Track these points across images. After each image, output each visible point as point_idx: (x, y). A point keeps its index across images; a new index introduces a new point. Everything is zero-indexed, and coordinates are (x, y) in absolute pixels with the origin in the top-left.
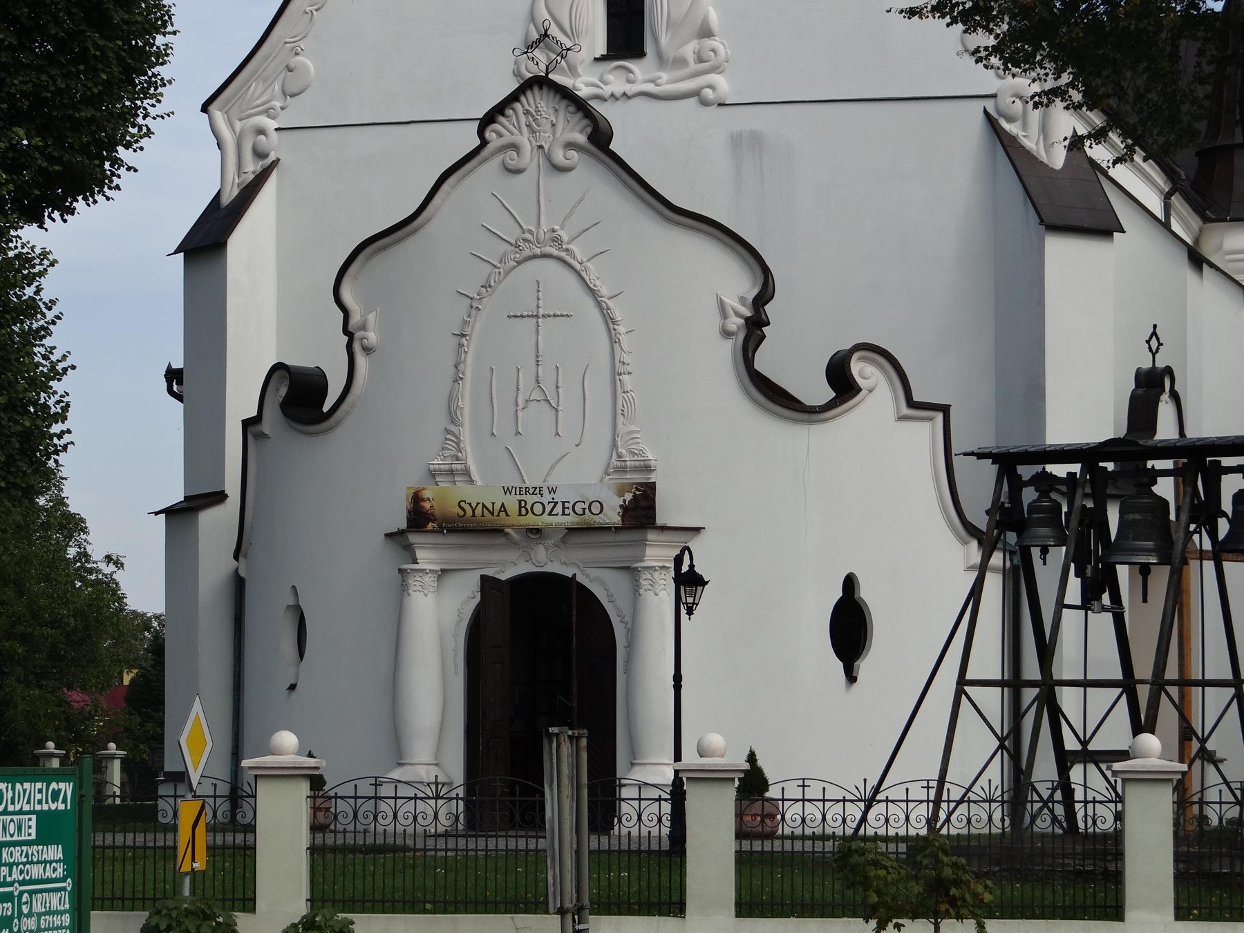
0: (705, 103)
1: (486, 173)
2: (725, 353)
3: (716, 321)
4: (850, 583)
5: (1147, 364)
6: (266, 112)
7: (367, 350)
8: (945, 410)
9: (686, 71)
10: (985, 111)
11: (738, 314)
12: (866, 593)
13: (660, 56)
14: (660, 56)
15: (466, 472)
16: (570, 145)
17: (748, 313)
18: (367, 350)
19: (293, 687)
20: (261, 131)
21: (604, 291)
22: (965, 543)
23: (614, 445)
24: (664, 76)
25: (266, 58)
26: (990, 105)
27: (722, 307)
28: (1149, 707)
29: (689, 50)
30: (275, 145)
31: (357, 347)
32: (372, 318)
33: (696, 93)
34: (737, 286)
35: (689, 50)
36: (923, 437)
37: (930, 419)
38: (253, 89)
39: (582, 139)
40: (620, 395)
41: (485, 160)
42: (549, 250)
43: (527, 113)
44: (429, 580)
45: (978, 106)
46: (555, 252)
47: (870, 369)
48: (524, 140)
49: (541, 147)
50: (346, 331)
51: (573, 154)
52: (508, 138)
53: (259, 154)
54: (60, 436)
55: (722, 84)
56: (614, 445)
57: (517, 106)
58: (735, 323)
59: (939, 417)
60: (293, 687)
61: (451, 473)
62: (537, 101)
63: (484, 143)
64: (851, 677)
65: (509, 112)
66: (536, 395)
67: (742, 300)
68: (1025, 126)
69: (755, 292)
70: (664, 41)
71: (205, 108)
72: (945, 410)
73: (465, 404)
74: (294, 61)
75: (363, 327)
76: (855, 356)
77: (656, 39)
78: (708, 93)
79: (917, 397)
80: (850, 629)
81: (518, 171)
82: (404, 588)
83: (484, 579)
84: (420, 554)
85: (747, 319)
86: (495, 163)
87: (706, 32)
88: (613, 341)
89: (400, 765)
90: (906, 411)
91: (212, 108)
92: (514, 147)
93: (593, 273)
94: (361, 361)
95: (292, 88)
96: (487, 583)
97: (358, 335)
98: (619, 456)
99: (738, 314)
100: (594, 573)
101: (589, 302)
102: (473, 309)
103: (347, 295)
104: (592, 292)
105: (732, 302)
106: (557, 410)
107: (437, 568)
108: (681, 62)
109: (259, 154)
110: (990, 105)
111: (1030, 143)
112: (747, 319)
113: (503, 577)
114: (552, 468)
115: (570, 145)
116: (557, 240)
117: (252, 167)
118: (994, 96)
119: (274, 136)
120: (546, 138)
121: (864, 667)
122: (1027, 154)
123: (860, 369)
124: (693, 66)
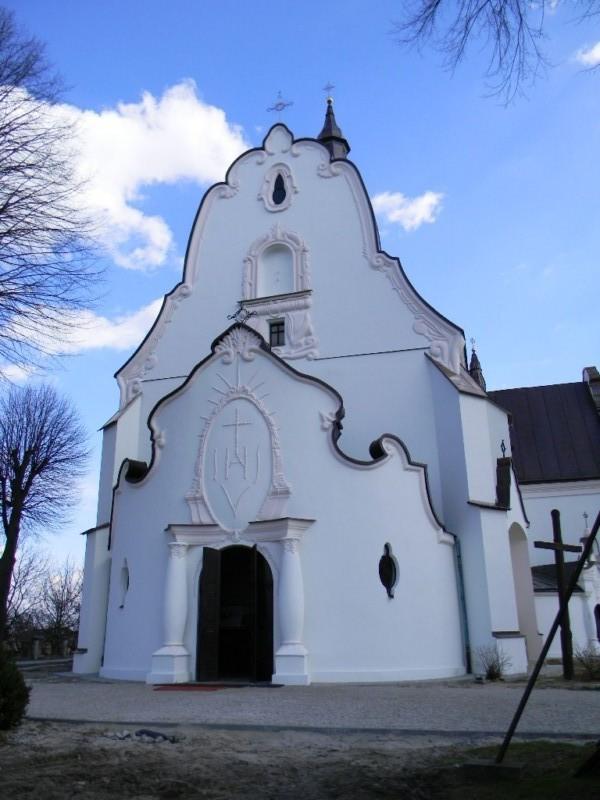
0: (309, 359)
1: (214, 366)
2: (323, 439)
3: (318, 424)
4: (387, 547)
5: (501, 456)
6: (138, 376)
7: (161, 447)
8: (425, 467)
9: (300, 349)
10: (426, 355)
11: (329, 420)
12: (395, 553)
13: (291, 344)
14: (291, 344)
15: (202, 498)
16: (252, 350)
17: (333, 419)
18: (161, 447)
19: (122, 607)
20: (136, 383)
21: (267, 412)
22: (438, 530)
23: (272, 481)
24: (293, 351)
25: (270, 555)
26: (427, 351)
27: (322, 418)
28: (165, 654)
29: (302, 341)
30: (141, 387)
31: (156, 446)
32: (163, 433)
33: (306, 356)
34: (328, 409)
35: (302, 341)
36: (415, 479)
37: (418, 471)
38: (133, 368)
39: (256, 347)
40: (274, 458)
41: (214, 360)
42: (241, 395)
43: (233, 339)
44: (183, 550)
45: (422, 352)
46: (244, 396)
47: (390, 446)
48: (232, 350)
49: (238, 353)
50: (152, 439)
51: (252, 354)
52: (224, 350)
53: (135, 391)
54: (69, 516)
55: (317, 353)
56: (272, 481)
57: (229, 337)
58: (328, 424)
59: (422, 470)
60: (122, 607)
61: (195, 499)
62: (238, 334)
63: (213, 353)
64: (391, 596)
65: (225, 339)
66: (235, 461)
67: (331, 414)
68: (443, 359)
69: (338, 409)
70: (292, 338)
71: (115, 376)
72: (425, 467)
73: (202, 467)
74: (150, 357)
75: (160, 437)
76: (384, 440)
77: (289, 338)
78: (310, 356)
79: (413, 459)
80: (388, 570)
81: (228, 363)
82: (169, 554)
83: (208, 553)
84: (178, 537)
85: (334, 422)
86: (219, 361)
87: (309, 334)
88: (271, 434)
89: (165, 646)
90: (409, 466)
91: (119, 376)
92: (227, 353)
93: (262, 406)
94: (158, 452)
95: (149, 366)
96: (208, 553)
97: (157, 440)
98: (274, 487)
99: (329, 420)
100: (266, 545)
101: (260, 420)
102: (207, 422)
103: (154, 424)
104: (262, 413)
105: (326, 414)
106: (244, 467)
107: (187, 544)
108: (299, 345)
109: (135, 391)
110: (427, 351)
111: (446, 364)
112: (334, 422)
113: (218, 548)
114: (173, 291)
115: (252, 350)
116: (245, 391)
117: (131, 396)
118: (429, 348)
119: (141, 385)
120: (241, 348)
121: (396, 590)
122: (446, 368)
123: (386, 446)
124: (304, 347)
